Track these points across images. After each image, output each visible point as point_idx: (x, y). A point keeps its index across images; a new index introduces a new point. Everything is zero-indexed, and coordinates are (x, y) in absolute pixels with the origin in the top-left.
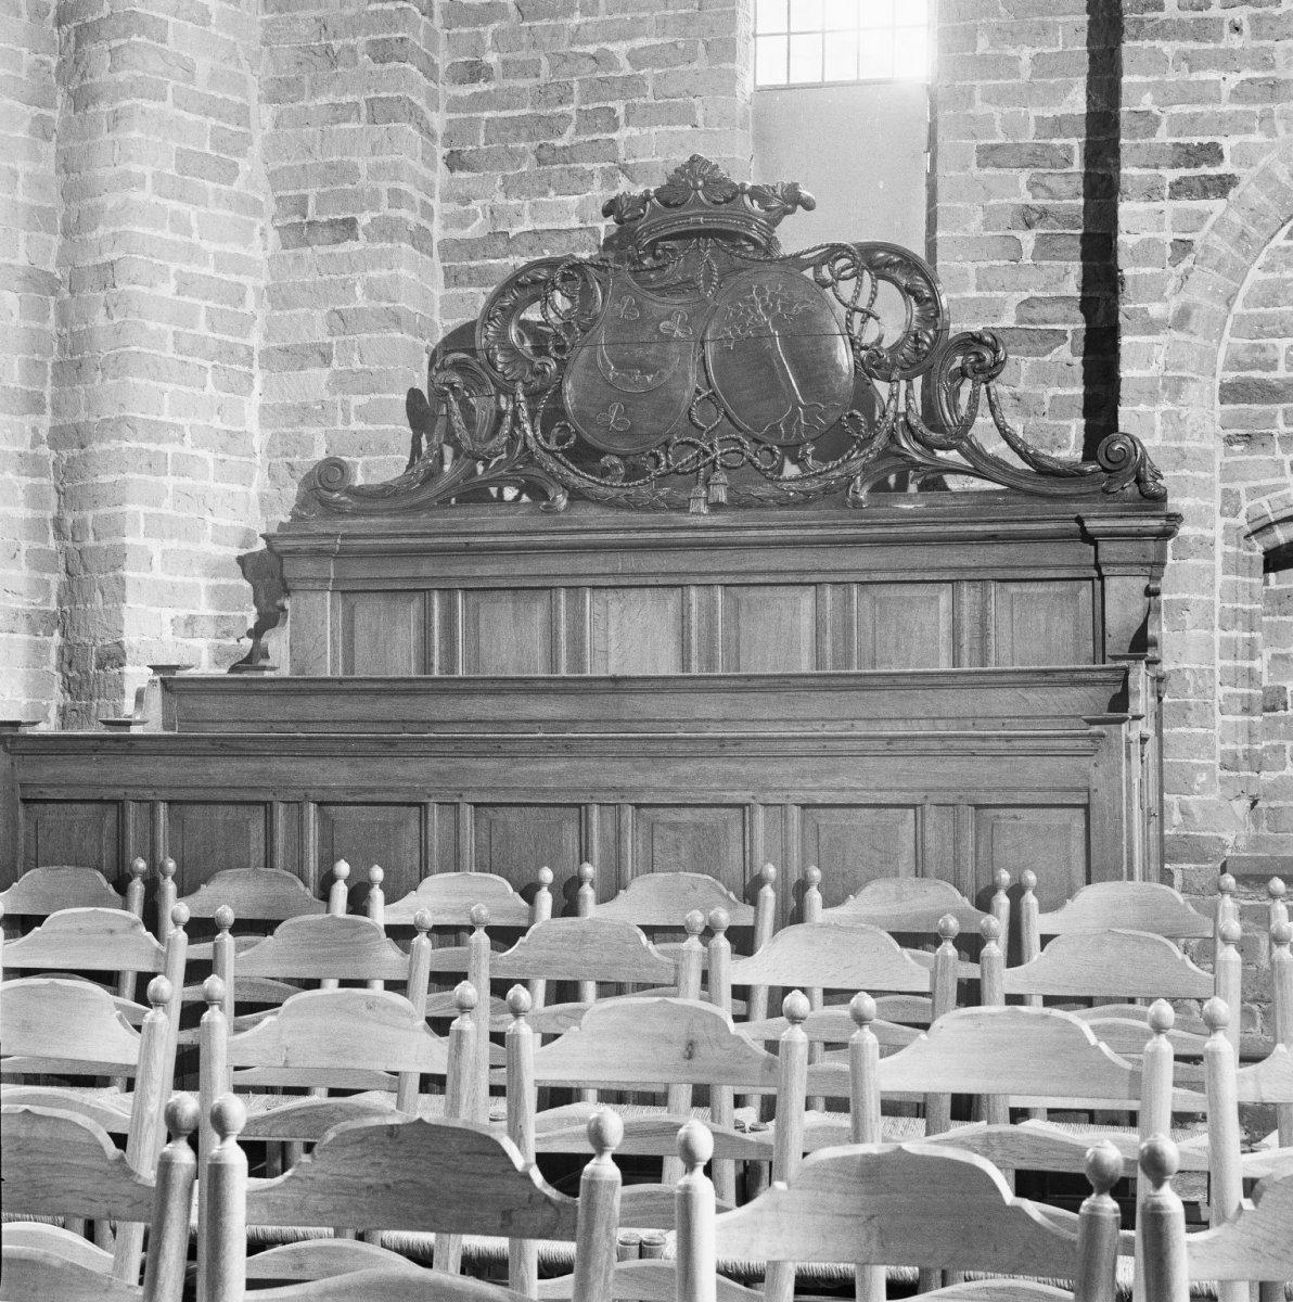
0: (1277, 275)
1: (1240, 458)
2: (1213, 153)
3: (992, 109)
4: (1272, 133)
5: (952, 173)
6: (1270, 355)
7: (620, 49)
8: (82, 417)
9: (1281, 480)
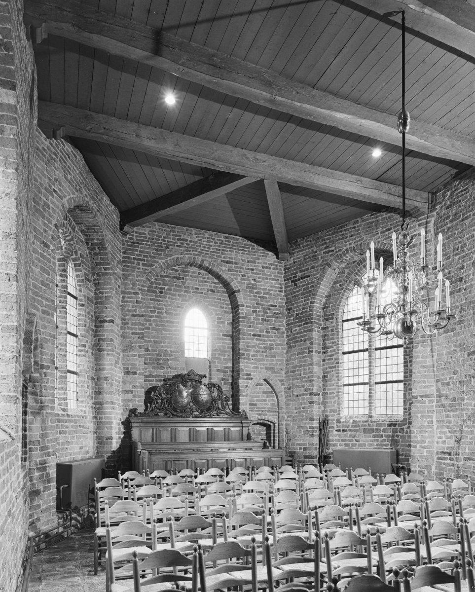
2: (250, 375)
7: (169, 350)
8: (101, 400)
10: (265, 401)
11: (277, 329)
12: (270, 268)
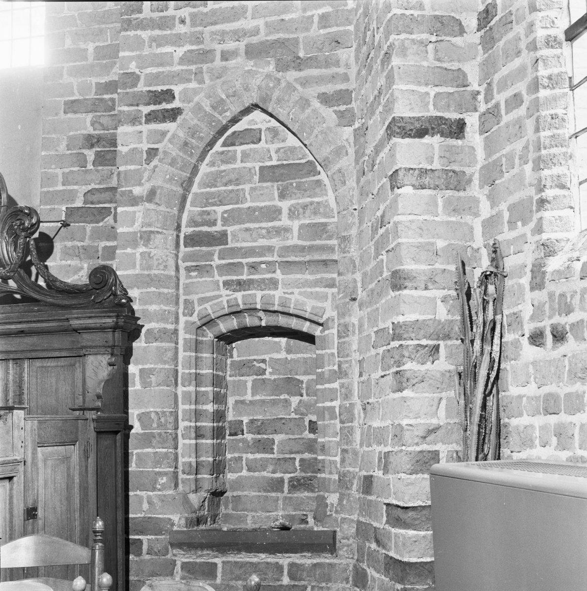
0: (216, 168)
1: (195, 280)
2: (169, 95)
3: (72, 80)
4: (201, 82)
5: (50, 118)
6: (212, 217)
9: (216, 293)
10: (273, 213)
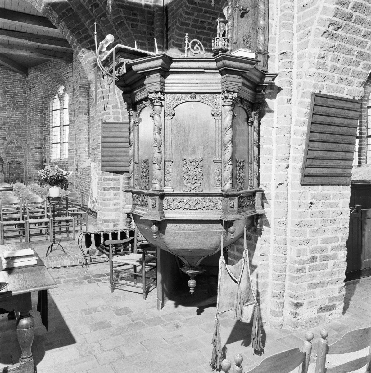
2: (6, 138)
11: (22, 114)
12: (18, 82)
